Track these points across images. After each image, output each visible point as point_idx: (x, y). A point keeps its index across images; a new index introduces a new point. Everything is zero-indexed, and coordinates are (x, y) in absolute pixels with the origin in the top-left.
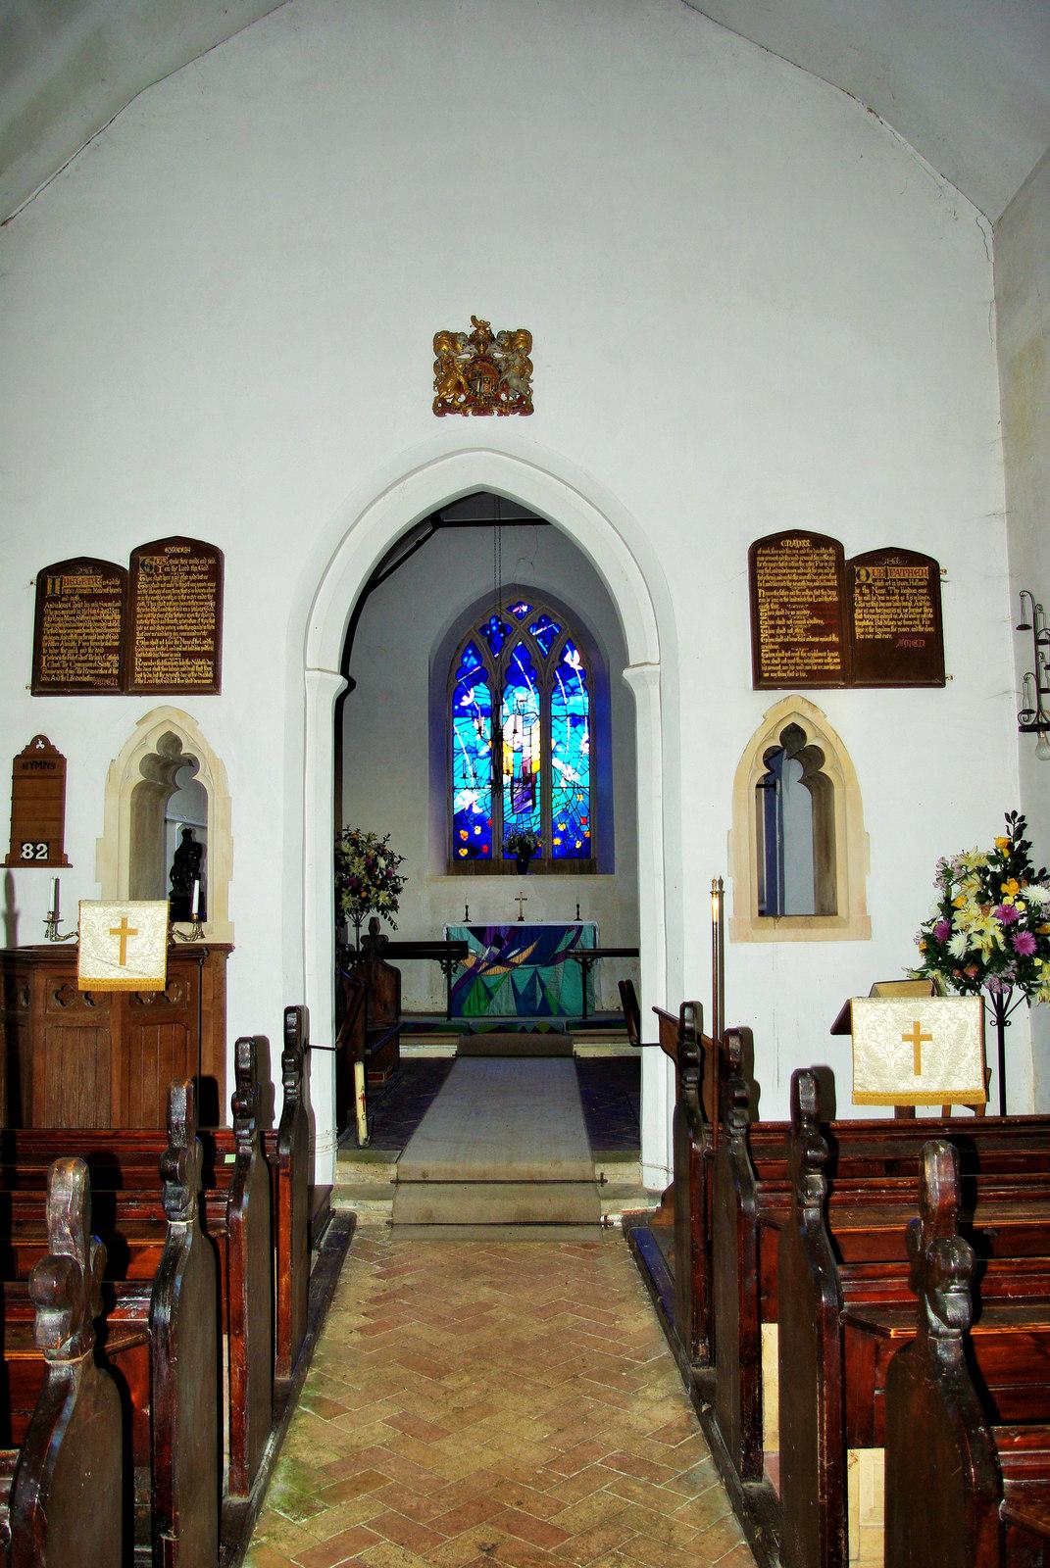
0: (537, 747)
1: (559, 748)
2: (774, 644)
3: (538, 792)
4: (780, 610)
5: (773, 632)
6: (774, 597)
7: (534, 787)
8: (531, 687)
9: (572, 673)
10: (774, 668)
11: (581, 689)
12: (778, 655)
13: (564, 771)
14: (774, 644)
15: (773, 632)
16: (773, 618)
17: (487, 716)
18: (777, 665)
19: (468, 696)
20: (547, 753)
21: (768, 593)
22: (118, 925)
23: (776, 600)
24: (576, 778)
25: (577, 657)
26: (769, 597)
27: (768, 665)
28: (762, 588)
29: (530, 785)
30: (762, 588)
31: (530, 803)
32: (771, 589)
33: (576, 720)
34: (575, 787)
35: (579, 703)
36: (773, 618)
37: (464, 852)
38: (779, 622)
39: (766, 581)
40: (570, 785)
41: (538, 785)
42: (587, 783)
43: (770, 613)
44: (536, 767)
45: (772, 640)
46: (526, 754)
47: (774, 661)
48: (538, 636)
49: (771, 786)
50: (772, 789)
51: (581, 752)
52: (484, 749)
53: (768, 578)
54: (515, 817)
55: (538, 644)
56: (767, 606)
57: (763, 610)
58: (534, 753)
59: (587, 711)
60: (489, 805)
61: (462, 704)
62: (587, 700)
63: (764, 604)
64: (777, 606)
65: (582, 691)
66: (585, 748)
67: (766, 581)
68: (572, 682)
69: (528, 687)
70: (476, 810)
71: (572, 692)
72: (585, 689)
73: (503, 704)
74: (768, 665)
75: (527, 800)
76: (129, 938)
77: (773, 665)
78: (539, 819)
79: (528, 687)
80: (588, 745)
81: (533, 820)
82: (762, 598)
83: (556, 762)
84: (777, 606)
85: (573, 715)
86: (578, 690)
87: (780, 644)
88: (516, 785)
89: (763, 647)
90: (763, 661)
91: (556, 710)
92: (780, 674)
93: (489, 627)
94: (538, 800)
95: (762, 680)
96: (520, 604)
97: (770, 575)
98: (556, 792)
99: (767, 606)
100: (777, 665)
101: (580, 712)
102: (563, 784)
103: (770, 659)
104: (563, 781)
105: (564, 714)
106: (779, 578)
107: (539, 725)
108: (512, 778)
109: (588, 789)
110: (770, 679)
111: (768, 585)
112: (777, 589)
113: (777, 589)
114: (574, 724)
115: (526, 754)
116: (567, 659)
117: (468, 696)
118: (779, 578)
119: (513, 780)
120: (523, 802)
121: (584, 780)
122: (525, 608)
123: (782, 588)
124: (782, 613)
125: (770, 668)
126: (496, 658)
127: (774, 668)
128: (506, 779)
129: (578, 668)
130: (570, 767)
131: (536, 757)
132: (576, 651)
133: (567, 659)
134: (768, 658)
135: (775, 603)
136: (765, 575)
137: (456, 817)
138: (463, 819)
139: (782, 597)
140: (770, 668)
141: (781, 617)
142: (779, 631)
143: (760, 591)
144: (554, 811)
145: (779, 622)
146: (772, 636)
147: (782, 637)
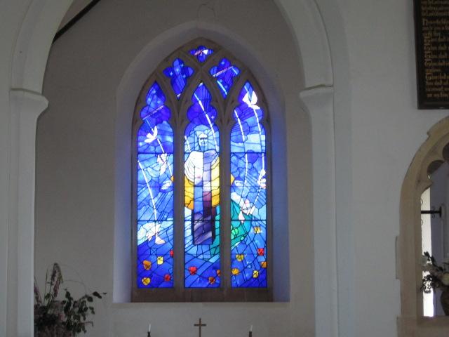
0: (216, 183)
1: (238, 183)
2: (436, 67)
3: (217, 224)
4: (442, 37)
5: (436, 57)
6: (436, 25)
7: (213, 221)
8: (211, 125)
9: (250, 112)
10: (437, 90)
11: (259, 128)
12: (440, 77)
13: (242, 204)
14: (436, 67)
15: (436, 57)
16: (435, 44)
17: (169, 154)
18: (440, 86)
19: (152, 133)
20: (226, 187)
21: (431, 23)
22: (202, 323)
23: (439, 28)
24: (253, 211)
25: (255, 98)
26: (432, 25)
27: (431, 87)
28: (426, 17)
29: (209, 218)
30: (426, 17)
31: (210, 234)
32: (434, 18)
33: (253, 156)
34: (251, 219)
35: (256, 141)
36: (435, 44)
37: (147, 281)
38: (441, 48)
39: (429, 12)
40: (248, 219)
41: (218, 217)
42: (264, 217)
43: (433, 40)
44: (215, 201)
45: (435, 64)
46: (207, 188)
47: (436, 84)
48: (218, 78)
49: (436, 212)
50: (437, 215)
51: (259, 187)
52: (167, 185)
53: (431, 8)
54: (195, 248)
55: (218, 85)
56: (430, 34)
57: (427, 37)
58: (214, 187)
59: (264, 148)
60: (171, 237)
61: (147, 141)
62: (263, 137)
63: (427, 32)
64: (439, 34)
65: (260, 129)
66: (262, 183)
67: (429, 12)
68: (250, 120)
69: (207, 125)
70: (159, 241)
71: (249, 130)
72: (263, 127)
73: (185, 141)
74: (431, 87)
75: (207, 232)
76: (202, 327)
77: (436, 87)
78: (218, 251)
79: (207, 125)
80: (264, 180)
81: (213, 251)
82: (426, 26)
83: (235, 196)
84: (439, 34)
85: (251, 153)
86: (256, 128)
87: (442, 68)
88: (197, 218)
89: (427, 70)
90: (427, 83)
91: (235, 148)
92: (442, 95)
93: (172, 69)
94: (217, 231)
95: (426, 100)
96: (201, 48)
97: (433, 5)
98: (235, 224)
99: (430, 34)
100: (440, 86)
101: (258, 148)
102: (241, 217)
103: (433, 81)
104: (241, 214)
105: (243, 151)
106: (441, 9)
107: (218, 161)
108: (193, 211)
109: (265, 222)
110: (434, 99)
111: (431, 14)
112: (440, 18)
113: (440, 18)
114: (252, 161)
115: (207, 188)
116: (246, 99)
117: (152, 133)
118: (441, 9)
119: (194, 214)
120: (202, 234)
121: (261, 213)
122: (206, 52)
123: (444, 17)
124: (444, 39)
125: (433, 89)
126: (179, 99)
127: (437, 90)
128: (188, 213)
129: (256, 108)
130: (247, 201)
131: (216, 192)
132: (254, 92)
133: (246, 99)
134: (432, 81)
135: (438, 31)
136: (428, 6)
137: (140, 247)
138: (142, 252)
139: (444, 25)
140: (433, 89)
141: (442, 44)
142: (441, 56)
143: (424, 20)
144: (233, 242)
145: (441, 48)
146: (435, 60)
147: (444, 62)
